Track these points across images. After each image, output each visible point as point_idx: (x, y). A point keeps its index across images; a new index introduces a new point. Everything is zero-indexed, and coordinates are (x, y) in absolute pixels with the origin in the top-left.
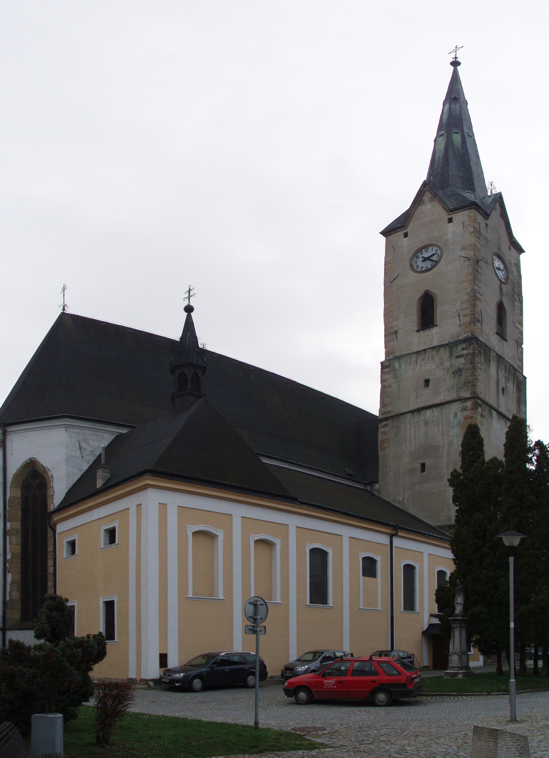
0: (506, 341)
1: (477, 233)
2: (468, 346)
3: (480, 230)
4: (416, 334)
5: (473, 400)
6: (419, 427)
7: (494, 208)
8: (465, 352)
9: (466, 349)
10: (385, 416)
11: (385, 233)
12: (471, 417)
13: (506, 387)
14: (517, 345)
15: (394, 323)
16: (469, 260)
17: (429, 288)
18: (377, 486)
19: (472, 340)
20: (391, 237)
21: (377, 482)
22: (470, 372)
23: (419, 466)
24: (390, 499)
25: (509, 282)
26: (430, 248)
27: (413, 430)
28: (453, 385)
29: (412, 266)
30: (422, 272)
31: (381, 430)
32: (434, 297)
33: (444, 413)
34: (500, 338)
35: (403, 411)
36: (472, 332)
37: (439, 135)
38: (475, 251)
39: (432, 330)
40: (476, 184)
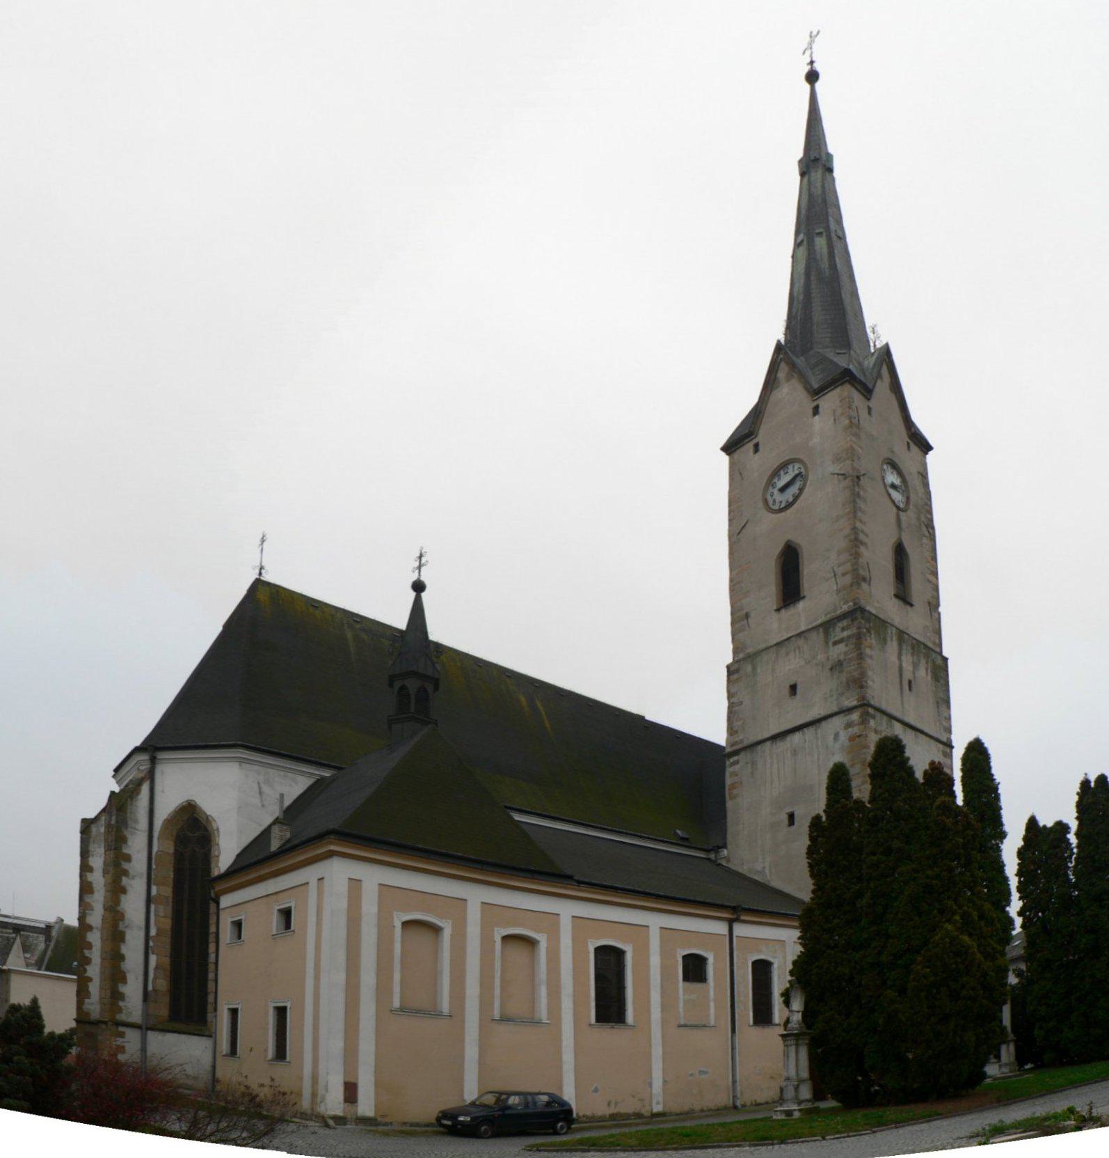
0: (912, 605)
1: (854, 426)
2: (850, 623)
3: (859, 420)
4: (775, 616)
5: (860, 710)
6: (784, 760)
7: (879, 376)
8: (846, 634)
9: (847, 629)
10: (735, 748)
11: (729, 448)
12: (859, 736)
13: (914, 677)
14: (930, 609)
15: (744, 601)
16: (845, 479)
17: (789, 537)
18: (725, 852)
19: (857, 613)
20: (736, 455)
21: (725, 846)
22: (854, 665)
23: (785, 818)
24: (743, 870)
25: (911, 507)
26: (790, 467)
27: (775, 766)
28: (831, 691)
29: (766, 501)
30: (781, 510)
31: (729, 770)
32: (799, 550)
33: (819, 735)
34: (901, 603)
35: (760, 738)
36: (854, 600)
37: (797, 245)
38: (853, 461)
39: (798, 605)
40: (853, 335)
